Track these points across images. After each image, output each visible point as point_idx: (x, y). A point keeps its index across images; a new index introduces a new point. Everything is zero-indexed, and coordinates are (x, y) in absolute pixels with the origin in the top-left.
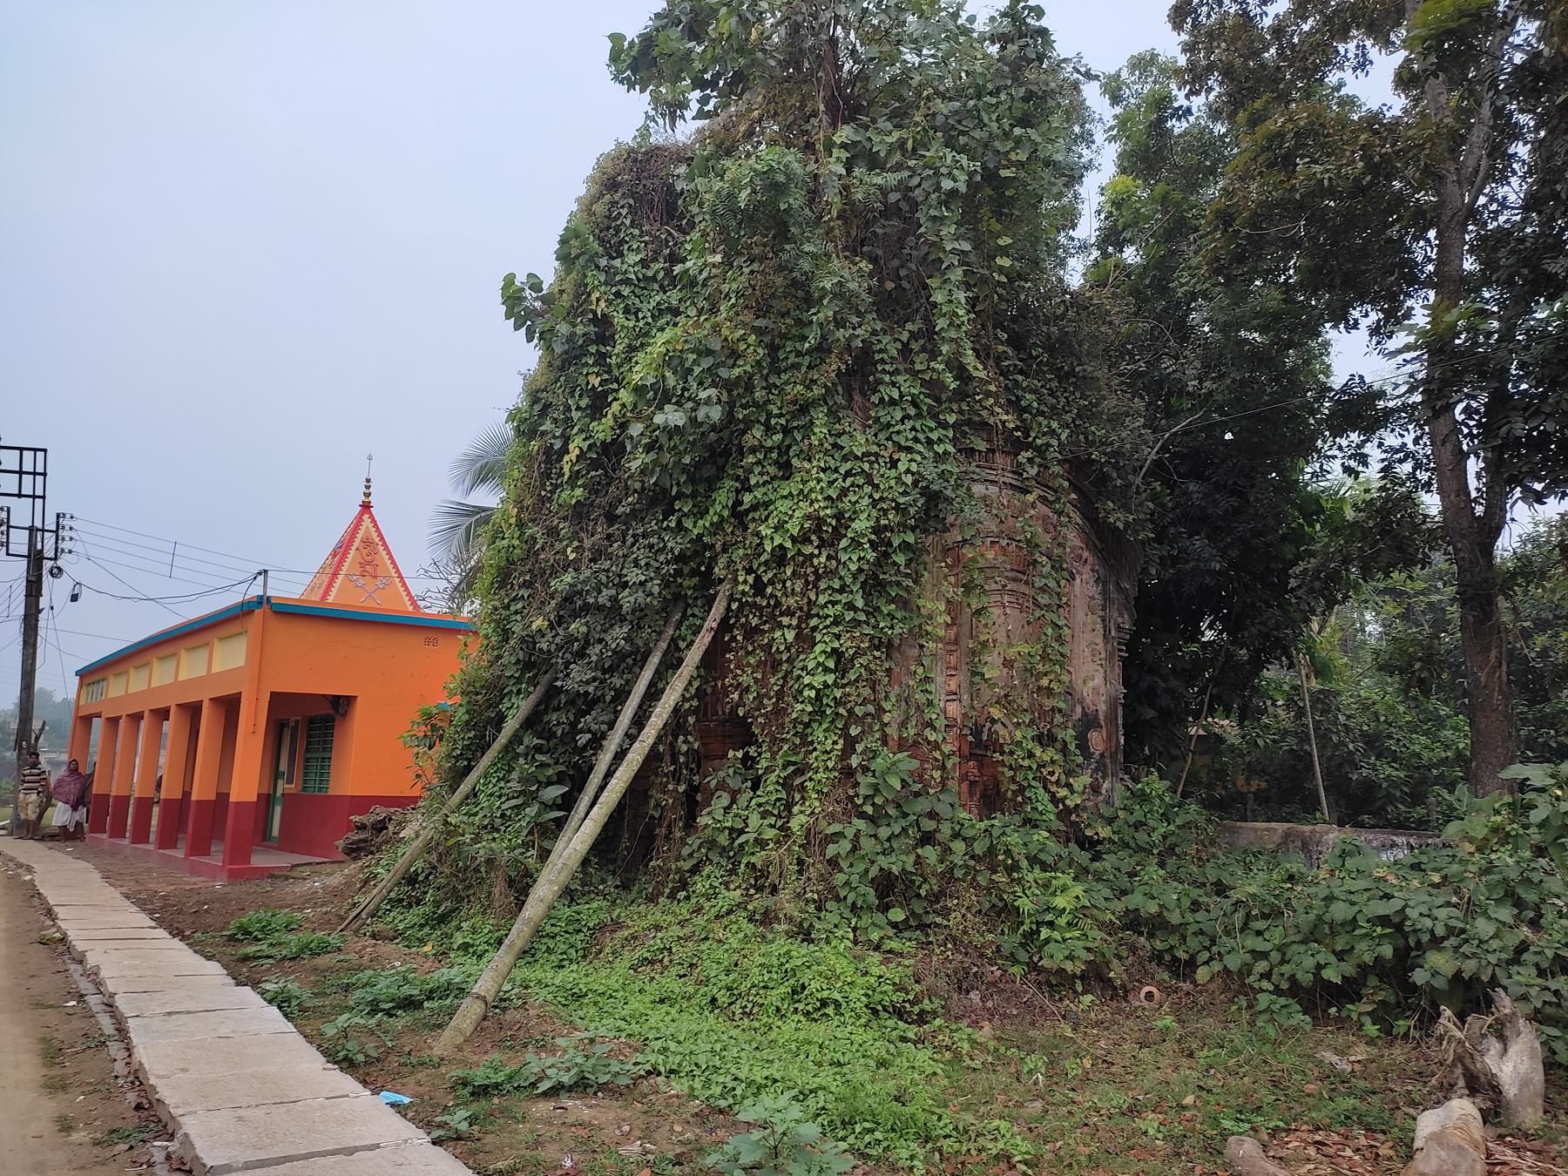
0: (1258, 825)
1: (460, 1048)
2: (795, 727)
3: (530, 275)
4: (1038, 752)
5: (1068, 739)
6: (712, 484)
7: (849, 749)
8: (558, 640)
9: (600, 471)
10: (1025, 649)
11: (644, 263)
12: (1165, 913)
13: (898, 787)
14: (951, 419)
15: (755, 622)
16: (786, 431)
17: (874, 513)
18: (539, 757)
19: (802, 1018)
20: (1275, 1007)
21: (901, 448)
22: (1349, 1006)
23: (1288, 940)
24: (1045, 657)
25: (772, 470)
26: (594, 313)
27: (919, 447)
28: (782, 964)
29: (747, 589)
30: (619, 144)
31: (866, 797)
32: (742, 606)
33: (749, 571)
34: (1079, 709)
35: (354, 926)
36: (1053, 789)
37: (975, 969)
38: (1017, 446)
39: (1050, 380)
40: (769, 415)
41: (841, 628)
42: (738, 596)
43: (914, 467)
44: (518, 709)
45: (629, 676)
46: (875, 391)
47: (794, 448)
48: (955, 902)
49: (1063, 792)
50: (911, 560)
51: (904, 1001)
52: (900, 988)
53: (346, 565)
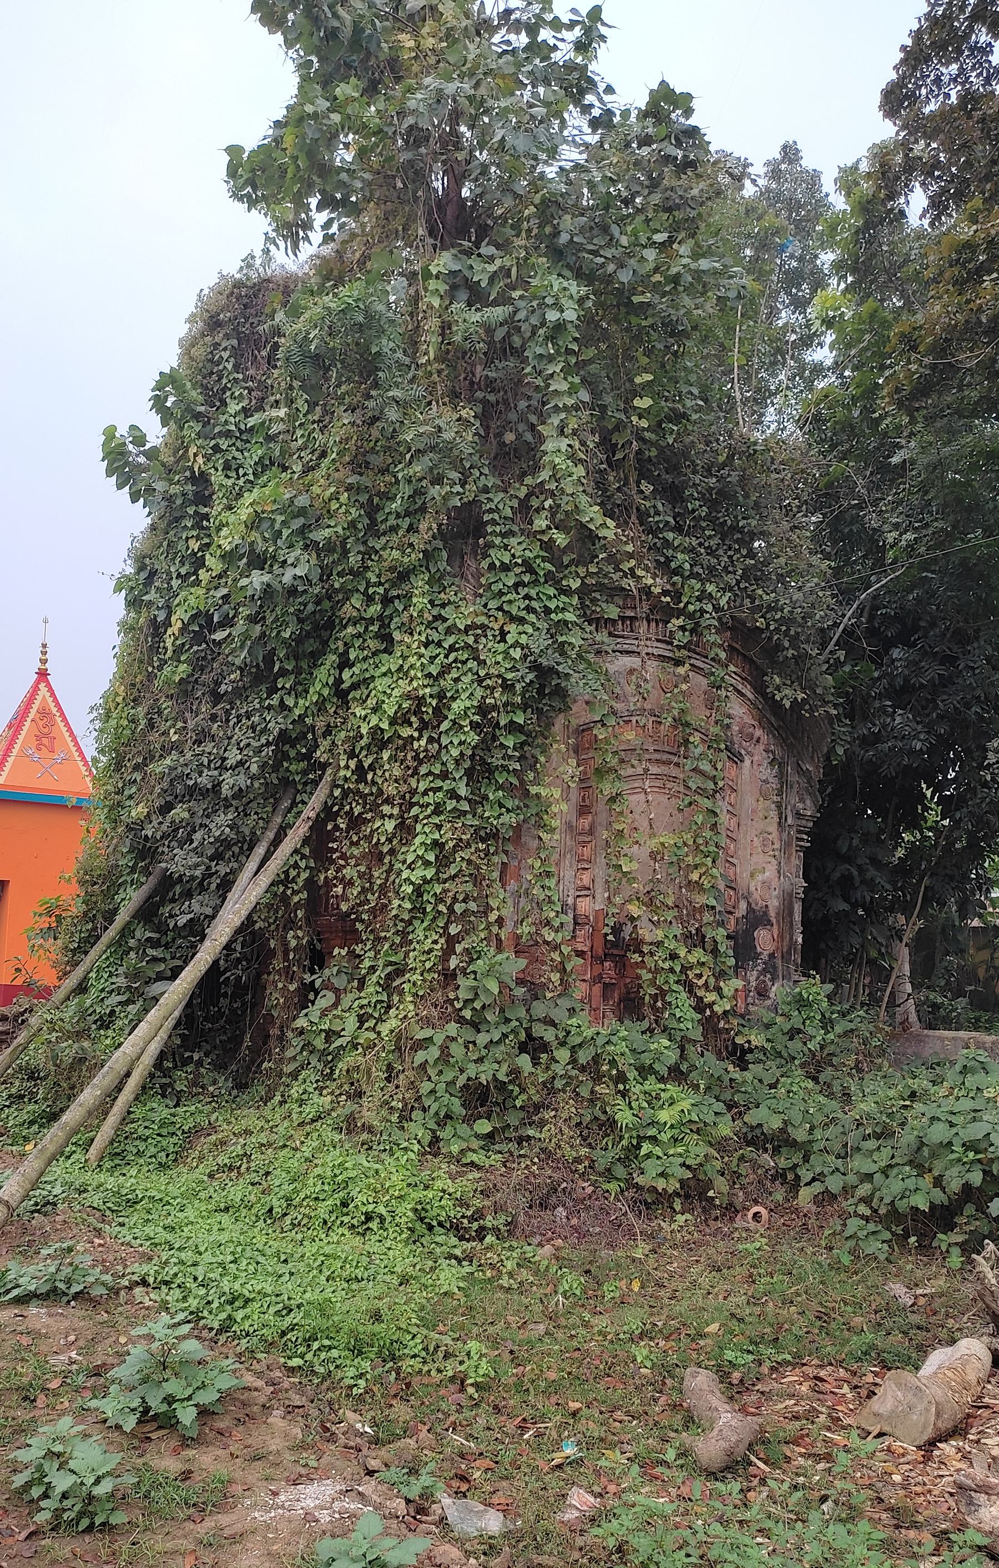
2: (396, 925)
3: (133, 428)
4: (682, 952)
5: (719, 939)
6: (315, 658)
7: (448, 951)
9: (204, 646)
10: (670, 840)
12: (790, 1129)
14: (575, 584)
16: (387, 601)
18: (151, 952)
19: (346, 1232)
20: (861, 1234)
21: (513, 619)
25: (373, 644)
26: (191, 469)
27: (532, 618)
28: (335, 1176)
29: (349, 774)
30: (223, 277)
31: (466, 1001)
32: (345, 793)
34: (743, 905)
36: (700, 993)
37: (564, 1185)
38: (668, 613)
39: (710, 537)
40: (368, 584)
41: (442, 817)
42: (341, 782)
43: (523, 639)
46: (486, 556)
47: (396, 620)
48: (553, 1113)
51: (463, 1217)
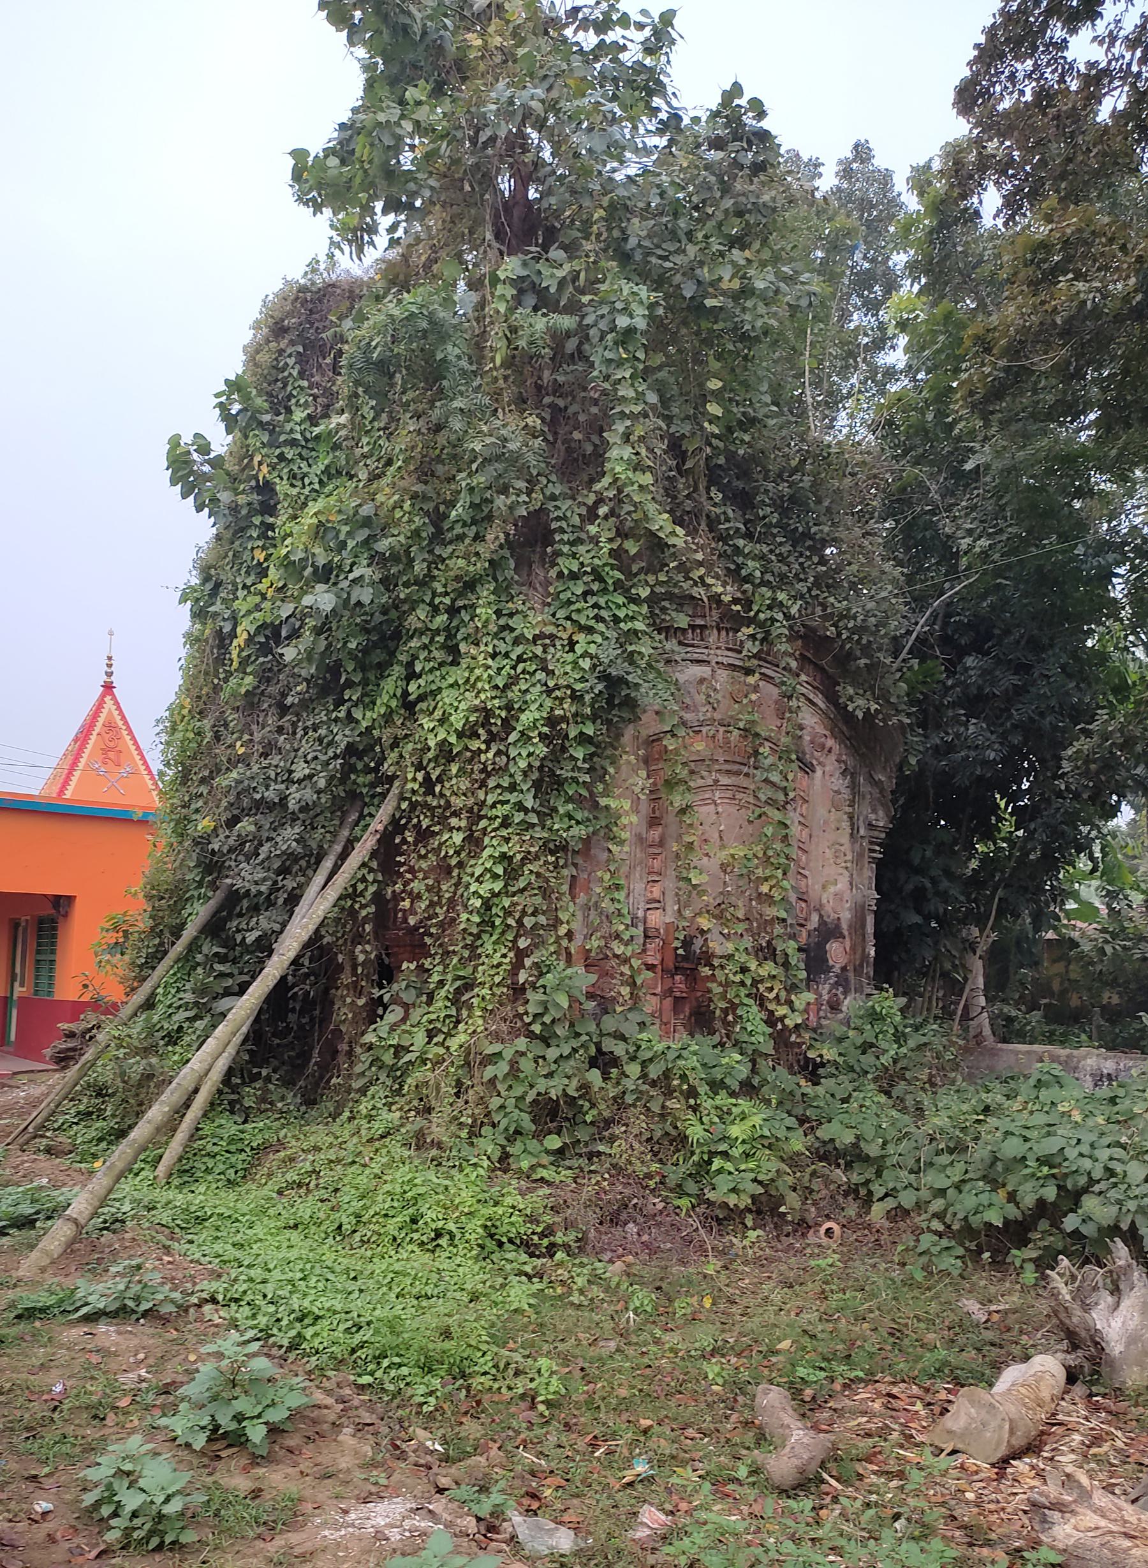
0: (1036, 1047)
1: (43, 1270)
3: (197, 436)
4: (753, 965)
5: (790, 951)
8: (231, 841)
11: (312, 420)
12: (862, 1144)
13: (566, 1005)
14: (644, 593)
15: (425, 823)
16: (453, 611)
17: (548, 703)
20: (935, 1250)
22: (1014, 1252)
23: (968, 1176)
24: (767, 860)
27: (601, 627)
31: (536, 1016)
33: (419, 767)
34: (815, 918)
35: (21, 1140)
39: (781, 544)
41: (510, 830)
42: (408, 795)
43: (592, 649)
44: (198, 914)
45: (303, 879)
46: (554, 564)
49: (782, 1011)
50: (592, 755)
52: (532, 1219)
53: (87, 751)
